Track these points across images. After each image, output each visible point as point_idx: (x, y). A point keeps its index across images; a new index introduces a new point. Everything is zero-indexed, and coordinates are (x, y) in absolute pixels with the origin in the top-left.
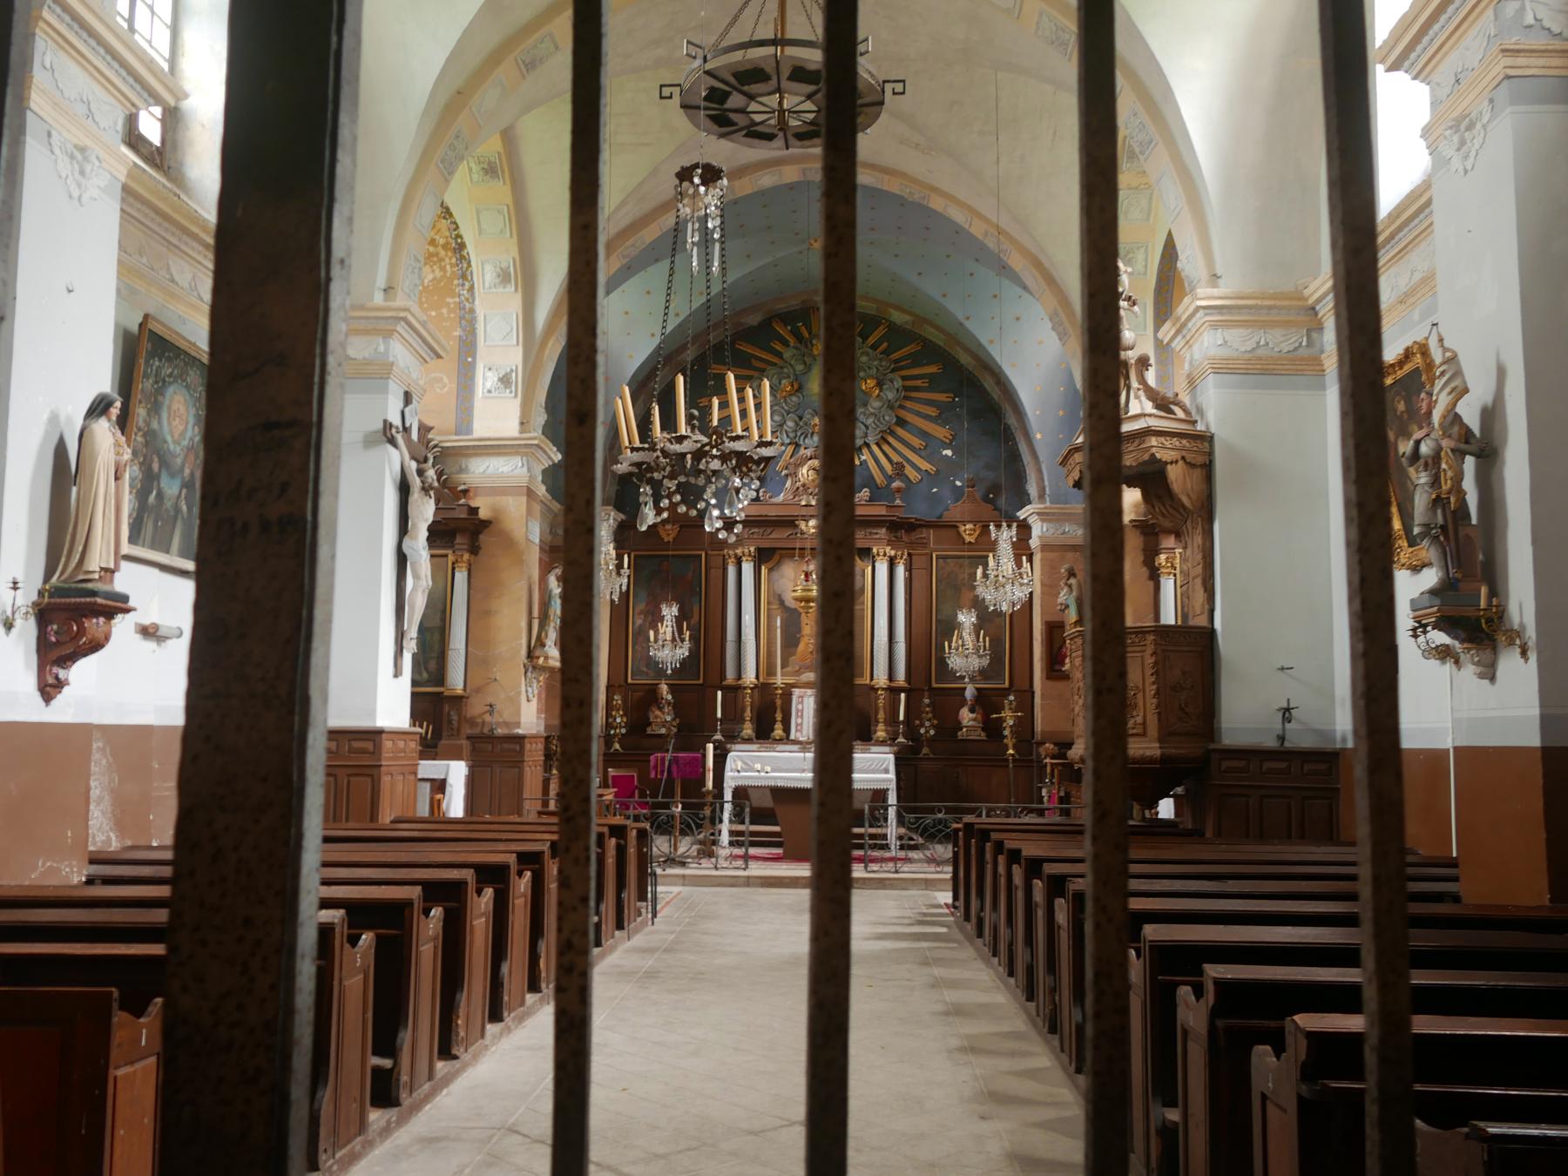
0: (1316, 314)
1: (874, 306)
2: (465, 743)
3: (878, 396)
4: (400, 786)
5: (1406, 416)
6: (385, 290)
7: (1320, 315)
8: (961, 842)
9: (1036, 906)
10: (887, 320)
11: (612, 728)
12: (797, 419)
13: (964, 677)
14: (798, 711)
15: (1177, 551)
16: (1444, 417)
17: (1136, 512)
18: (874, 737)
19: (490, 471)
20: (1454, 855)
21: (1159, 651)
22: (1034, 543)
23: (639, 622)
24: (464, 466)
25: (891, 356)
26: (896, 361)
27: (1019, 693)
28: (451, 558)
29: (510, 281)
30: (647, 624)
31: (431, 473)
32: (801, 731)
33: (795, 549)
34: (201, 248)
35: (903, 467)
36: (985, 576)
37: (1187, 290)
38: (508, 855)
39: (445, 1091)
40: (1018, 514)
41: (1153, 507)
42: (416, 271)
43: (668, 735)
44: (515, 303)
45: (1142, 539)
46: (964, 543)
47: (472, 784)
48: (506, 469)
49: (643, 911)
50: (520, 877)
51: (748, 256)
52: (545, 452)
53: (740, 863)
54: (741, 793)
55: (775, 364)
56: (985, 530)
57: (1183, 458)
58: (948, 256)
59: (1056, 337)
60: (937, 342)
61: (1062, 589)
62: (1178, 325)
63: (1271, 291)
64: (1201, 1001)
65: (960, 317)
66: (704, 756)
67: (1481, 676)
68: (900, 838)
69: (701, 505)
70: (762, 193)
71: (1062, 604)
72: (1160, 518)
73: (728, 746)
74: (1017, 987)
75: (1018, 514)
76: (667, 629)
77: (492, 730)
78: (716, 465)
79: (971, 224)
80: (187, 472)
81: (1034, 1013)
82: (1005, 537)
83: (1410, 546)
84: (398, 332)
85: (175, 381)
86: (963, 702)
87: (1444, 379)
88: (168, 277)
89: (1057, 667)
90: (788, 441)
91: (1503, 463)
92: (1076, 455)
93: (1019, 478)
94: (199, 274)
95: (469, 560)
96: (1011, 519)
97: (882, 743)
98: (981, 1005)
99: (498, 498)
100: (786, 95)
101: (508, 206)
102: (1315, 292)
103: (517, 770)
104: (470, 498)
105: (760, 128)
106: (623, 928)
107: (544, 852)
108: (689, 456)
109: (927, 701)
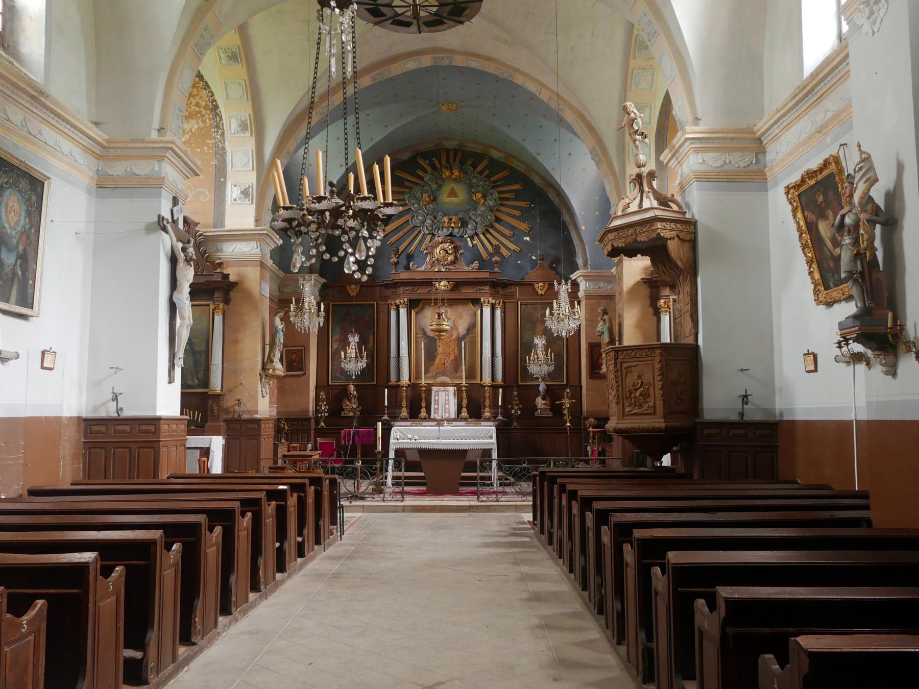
0: (761, 143)
1: (481, 147)
2: (222, 424)
3: (483, 203)
4: (174, 454)
5: (823, 205)
6: (158, 130)
7: (764, 143)
8: (538, 484)
9: (588, 529)
10: (489, 156)
12: (433, 219)
13: (538, 378)
15: (670, 297)
16: (862, 198)
17: (645, 274)
18: (483, 416)
19: (236, 251)
20: (857, 489)
21: (663, 360)
22: (581, 294)
23: (336, 346)
24: (219, 248)
25: (492, 178)
26: (494, 182)
27: (573, 387)
28: (212, 307)
29: (247, 129)
30: (341, 348)
31: (191, 250)
32: (438, 413)
33: (431, 299)
34: (28, 99)
35: (500, 248)
36: (552, 314)
37: (679, 128)
39: (186, 668)
40: (571, 276)
42: (179, 118)
43: (355, 417)
44: (251, 144)
49: (335, 531)
50: (243, 517)
51: (401, 115)
52: (271, 238)
53: (399, 496)
54: (400, 452)
55: (419, 184)
57: (678, 236)
58: (526, 115)
59: (595, 165)
62: (673, 151)
63: (733, 128)
64: (714, 613)
65: (535, 154)
66: (376, 430)
67: (887, 373)
69: (342, 253)
70: (408, 74)
71: (599, 332)
72: (663, 275)
73: (392, 423)
74: (576, 580)
75: (571, 276)
76: (352, 351)
77: (239, 416)
78: (351, 223)
79: (540, 93)
80: (21, 248)
81: (588, 600)
82: (564, 289)
83: (825, 290)
84: (167, 157)
85: (10, 187)
86: (538, 394)
87: (862, 173)
88: (5, 117)
90: (427, 232)
91: (902, 228)
93: (571, 254)
94: (27, 115)
95: (223, 308)
97: (488, 420)
102: (762, 127)
108: (327, 213)
109: (516, 393)
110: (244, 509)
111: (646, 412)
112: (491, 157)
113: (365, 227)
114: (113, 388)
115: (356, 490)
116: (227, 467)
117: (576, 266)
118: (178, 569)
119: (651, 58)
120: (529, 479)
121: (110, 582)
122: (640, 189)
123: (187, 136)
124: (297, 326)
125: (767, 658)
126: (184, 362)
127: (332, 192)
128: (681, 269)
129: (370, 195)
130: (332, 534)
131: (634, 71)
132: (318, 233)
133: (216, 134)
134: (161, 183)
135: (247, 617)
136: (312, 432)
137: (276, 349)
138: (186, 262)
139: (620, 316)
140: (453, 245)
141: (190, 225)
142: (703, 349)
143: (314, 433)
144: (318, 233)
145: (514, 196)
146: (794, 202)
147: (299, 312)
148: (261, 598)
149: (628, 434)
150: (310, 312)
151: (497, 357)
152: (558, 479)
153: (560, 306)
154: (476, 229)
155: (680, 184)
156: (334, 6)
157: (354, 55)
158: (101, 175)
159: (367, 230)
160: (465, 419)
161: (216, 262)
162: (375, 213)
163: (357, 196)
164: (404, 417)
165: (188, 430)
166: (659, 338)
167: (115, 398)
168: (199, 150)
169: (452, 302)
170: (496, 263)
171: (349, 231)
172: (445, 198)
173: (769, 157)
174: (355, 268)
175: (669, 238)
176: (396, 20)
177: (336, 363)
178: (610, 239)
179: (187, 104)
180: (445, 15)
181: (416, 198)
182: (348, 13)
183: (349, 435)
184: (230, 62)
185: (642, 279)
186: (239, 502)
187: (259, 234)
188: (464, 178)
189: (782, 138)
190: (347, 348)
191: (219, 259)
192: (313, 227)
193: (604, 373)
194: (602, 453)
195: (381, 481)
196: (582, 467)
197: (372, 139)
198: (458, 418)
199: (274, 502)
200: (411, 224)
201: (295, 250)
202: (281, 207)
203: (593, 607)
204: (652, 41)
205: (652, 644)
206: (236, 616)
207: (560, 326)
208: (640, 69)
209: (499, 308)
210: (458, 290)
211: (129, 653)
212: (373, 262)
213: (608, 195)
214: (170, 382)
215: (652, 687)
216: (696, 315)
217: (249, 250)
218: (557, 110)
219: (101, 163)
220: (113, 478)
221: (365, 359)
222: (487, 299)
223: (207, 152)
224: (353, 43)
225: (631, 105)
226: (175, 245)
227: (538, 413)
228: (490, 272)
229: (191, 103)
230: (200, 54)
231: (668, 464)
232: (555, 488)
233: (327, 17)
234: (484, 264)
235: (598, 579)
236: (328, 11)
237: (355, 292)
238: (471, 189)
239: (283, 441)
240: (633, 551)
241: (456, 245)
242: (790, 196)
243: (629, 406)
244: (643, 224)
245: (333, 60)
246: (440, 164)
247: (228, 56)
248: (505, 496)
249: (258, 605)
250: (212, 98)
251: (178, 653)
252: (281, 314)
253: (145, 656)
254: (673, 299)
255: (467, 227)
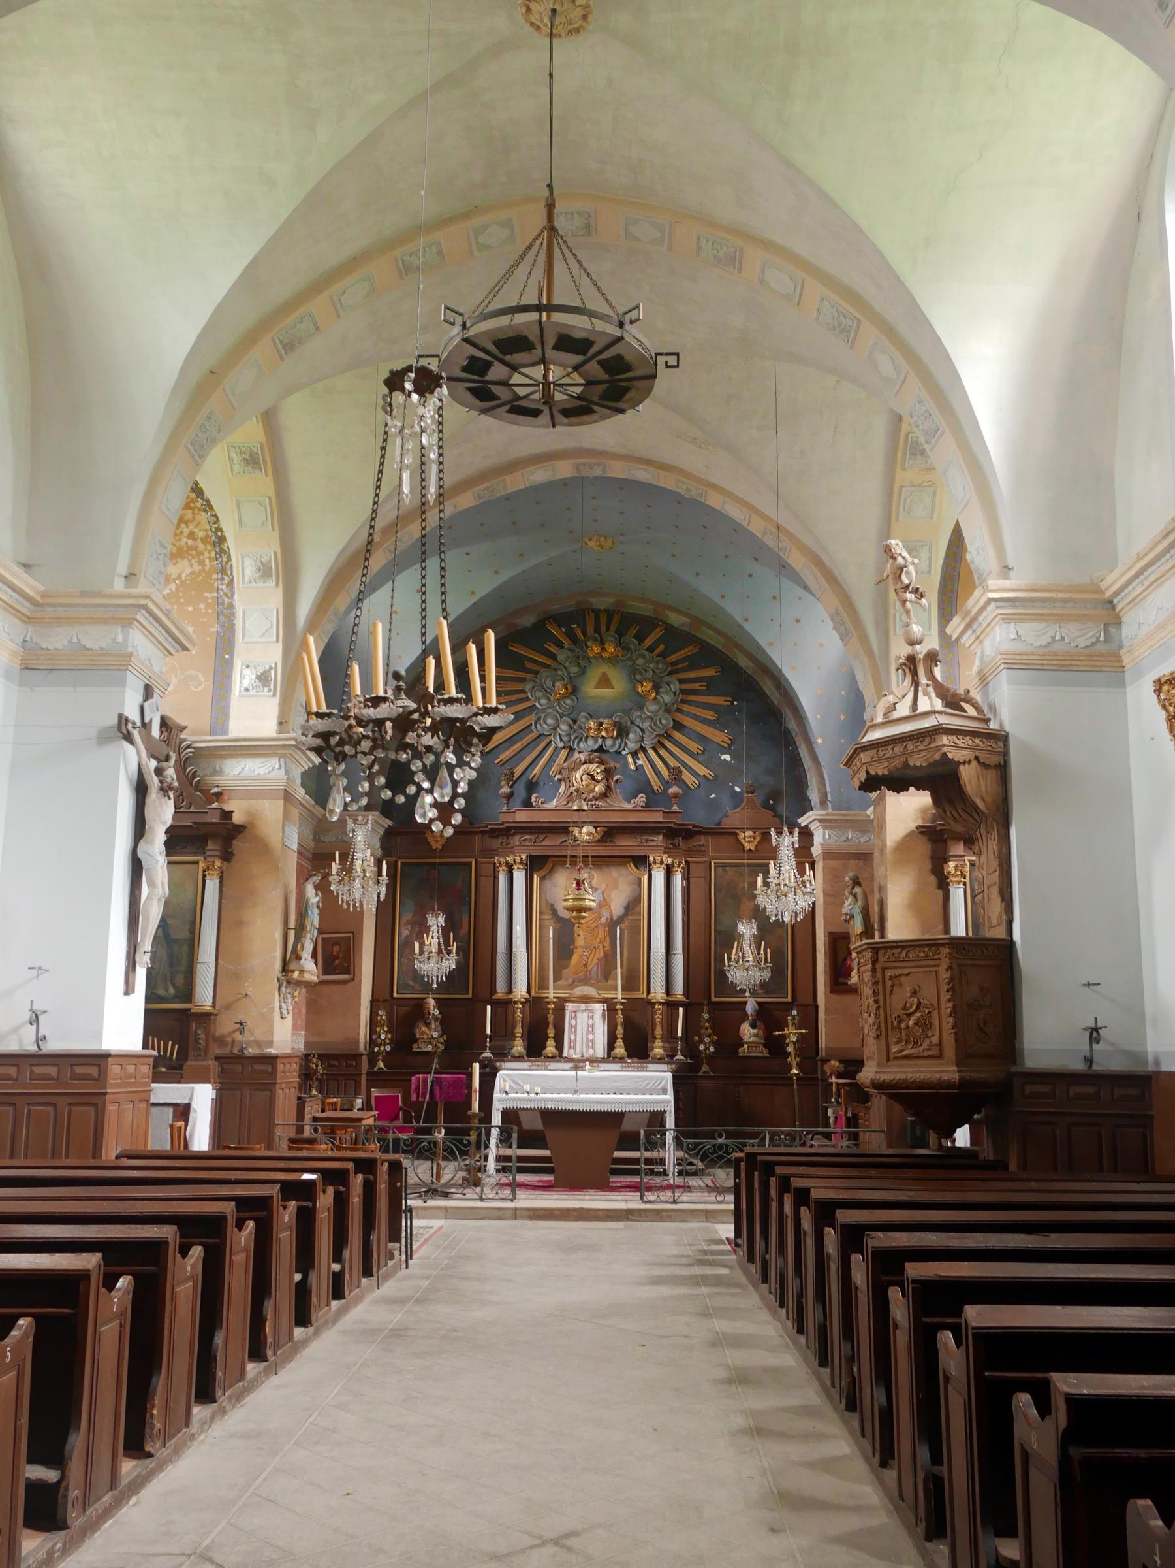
0: (1114, 608)
2: (211, 1063)
3: (655, 699)
7: (1118, 609)
8: (743, 1175)
9: (829, 1257)
10: (664, 622)
11: (377, 1045)
12: (571, 723)
13: (744, 991)
14: (571, 1026)
15: (966, 858)
17: (923, 819)
18: (651, 1054)
19: (246, 772)
21: (954, 965)
22: (816, 850)
23: (406, 933)
24: (218, 768)
25: (669, 659)
26: (673, 664)
27: (802, 1007)
28: (202, 865)
29: (271, 575)
30: (414, 935)
31: (171, 772)
32: (575, 1048)
33: (566, 856)
35: (681, 772)
36: (766, 884)
38: (226, 1203)
39: (133, 1500)
40: (799, 821)
41: (945, 812)
42: (161, 558)
43: (435, 1052)
44: (274, 598)
45: (929, 846)
46: (744, 851)
47: (220, 1109)
48: (262, 771)
49: (396, 1253)
51: (521, 555)
53: (507, 1192)
54: (510, 1116)
56: (766, 836)
60: (716, 645)
61: (847, 899)
62: (968, 619)
63: (1067, 584)
64: (1047, 1418)
65: (740, 621)
68: (679, 1162)
69: (412, 790)
70: (537, 489)
71: (846, 914)
72: (952, 822)
73: (498, 1064)
74: (808, 1348)
75: (799, 821)
76: (433, 941)
77: (242, 1050)
78: (428, 740)
81: (829, 1383)
82: (787, 843)
84: (138, 621)
86: (744, 1016)
89: (841, 980)
90: (561, 745)
92: (862, 755)
96: (792, 826)
97: (660, 1060)
98: (767, 1370)
99: (253, 801)
100: (552, 366)
101: (269, 498)
103: (268, 1093)
104: (223, 802)
105: (522, 403)
106: (372, 1275)
107: (272, 1197)
108: (389, 724)
109: (706, 1016)
110: (242, 1215)
111: (926, 1054)
112: (668, 624)
113: (451, 748)
114: (32, 1001)
115: (435, 1181)
116: (219, 1137)
117: (808, 803)
118: (125, 1321)
119: (930, 469)
120: (728, 1163)
121: (7, 1346)
122: (913, 681)
123: (173, 586)
124: (342, 899)
125: (1143, 1506)
126: (153, 959)
127: (398, 689)
128: (982, 812)
129: (460, 696)
130: (392, 1257)
131: (904, 489)
132: (373, 757)
133: (220, 582)
134: (125, 663)
135: (241, 1406)
136: (364, 1078)
137: (305, 936)
138: (162, 792)
139: (882, 889)
140: (603, 767)
141: (171, 732)
142: (1022, 954)
143: (367, 1080)
144: (373, 757)
145: (705, 688)
146: (1170, 705)
147: (345, 875)
148: (267, 1372)
149: (894, 1091)
150: (365, 876)
151: (675, 954)
152: (776, 1167)
153: (780, 870)
154: (643, 740)
155: (979, 673)
156: (410, 389)
157: (441, 467)
158: (29, 650)
159: (453, 752)
160: (620, 1058)
161: (212, 791)
162: (468, 724)
163: (439, 697)
164: (517, 1055)
165: (153, 1073)
166: (947, 929)
167: (35, 1019)
168: (190, 609)
169: (600, 861)
170: (675, 797)
171: (425, 753)
172: (591, 690)
173: (1127, 631)
174: (434, 814)
175: (961, 761)
176: (515, 406)
177: (406, 961)
178: (863, 762)
179: (176, 535)
180: (595, 399)
181: (544, 688)
182: (433, 401)
183: (425, 1085)
184: (247, 468)
185: (918, 827)
186: (234, 1203)
187: (283, 745)
188: (622, 656)
189: (1150, 599)
190: (425, 935)
191: (218, 786)
192: (366, 745)
193: (855, 984)
194: (852, 1121)
195: (478, 1163)
196: (817, 1145)
197: (473, 593)
198: (610, 1055)
199: (294, 1202)
200: (535, 732)
201: (334, 784)
202: (312, 714)
203: (838, 1398)
204: (932, 444)
205: (941, 1467)
206: (224, 1404)
207: (781, 905)
208: (912, 486)
209: (678, 872)
210: (611, 841)
211: (37, 1472)
212: (463, 806)
214: (127, 993)
215: (941, 1547)
216: (1009, 890)
217: (267, 771)
218: (776, 550)
219: (31, 629)
220: (26, 1157)
221: (454, 954)
222: (659, 858)
223: (203, 611)
224: (439, 449)
225: (897, 544)
226: (144, 763)
227: (743, 1051)
228: (664, 812)
229: (182, 533)
230: (199, 456)
231: (966, 1143)
232: (771, 1182)
233: (397, 407)
234: (654, 799)
235: (846, 1347)
236: (400, 397)
237: (441, 843)
238: (634, 674)
239: (314, 1092)
240: (905, 1301)
241: (608, 766)
242: (1162, 696)
243: (898, 1042)
244: (918, 738)
245: (406, 476)
246: (585, 634)
247: (244, 459)
248: (689, 1194)
249: (261, 1385)
250: (216, 525)
251: (120, 1473)
252: (317, 879)
253: (63, 1477)
254: (970, 861)
255: (627, 737)
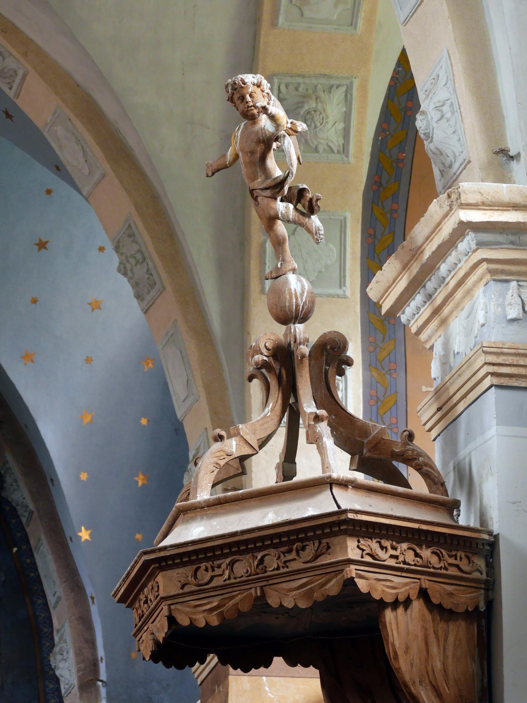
37: (439, 184)
57: (423, 594)
62: (415, 269)
175: (388, 599)
178: (162, 594)
213: (179, 414)
244: (293, 542)
